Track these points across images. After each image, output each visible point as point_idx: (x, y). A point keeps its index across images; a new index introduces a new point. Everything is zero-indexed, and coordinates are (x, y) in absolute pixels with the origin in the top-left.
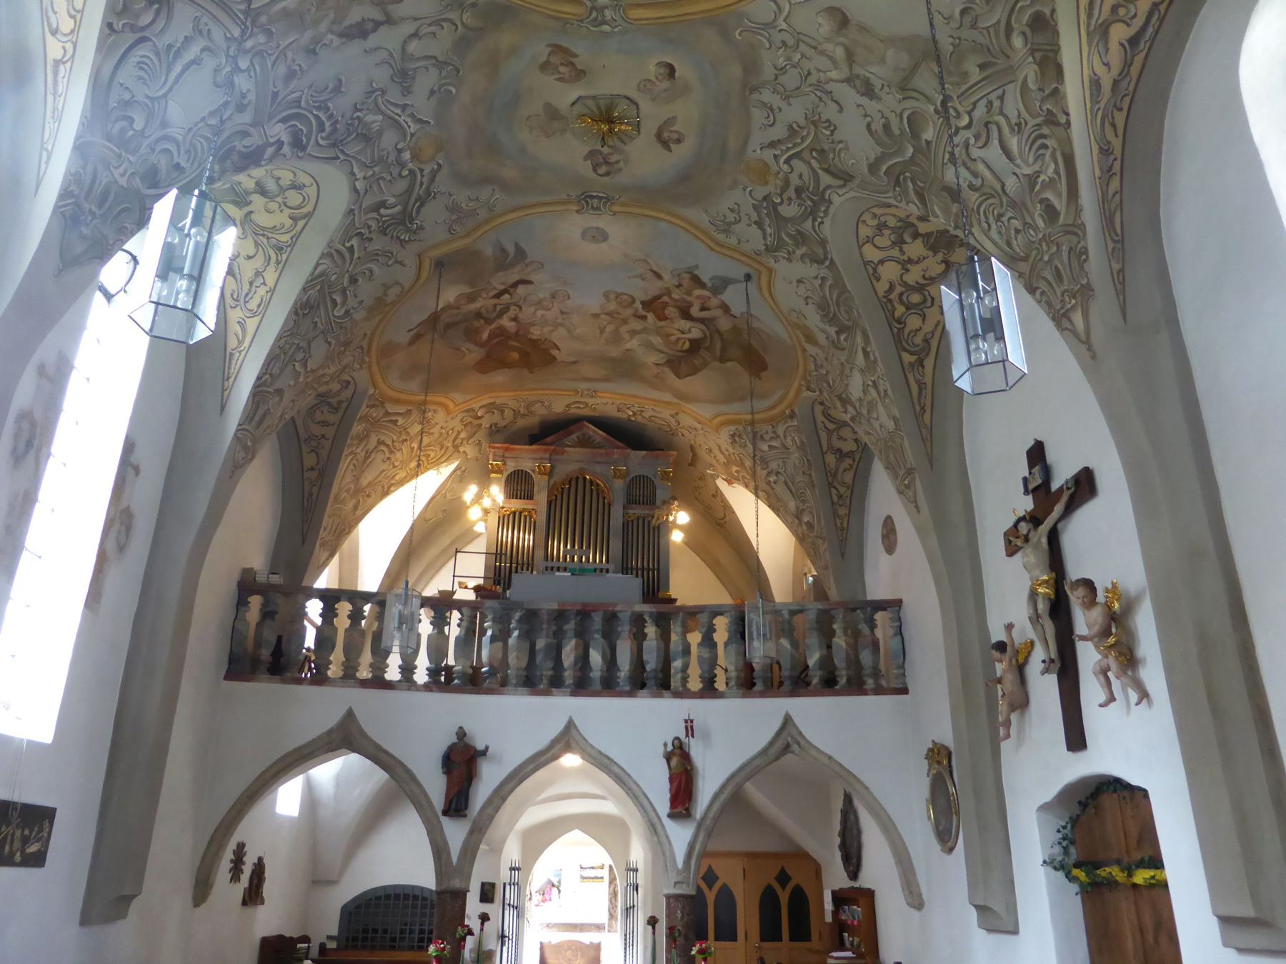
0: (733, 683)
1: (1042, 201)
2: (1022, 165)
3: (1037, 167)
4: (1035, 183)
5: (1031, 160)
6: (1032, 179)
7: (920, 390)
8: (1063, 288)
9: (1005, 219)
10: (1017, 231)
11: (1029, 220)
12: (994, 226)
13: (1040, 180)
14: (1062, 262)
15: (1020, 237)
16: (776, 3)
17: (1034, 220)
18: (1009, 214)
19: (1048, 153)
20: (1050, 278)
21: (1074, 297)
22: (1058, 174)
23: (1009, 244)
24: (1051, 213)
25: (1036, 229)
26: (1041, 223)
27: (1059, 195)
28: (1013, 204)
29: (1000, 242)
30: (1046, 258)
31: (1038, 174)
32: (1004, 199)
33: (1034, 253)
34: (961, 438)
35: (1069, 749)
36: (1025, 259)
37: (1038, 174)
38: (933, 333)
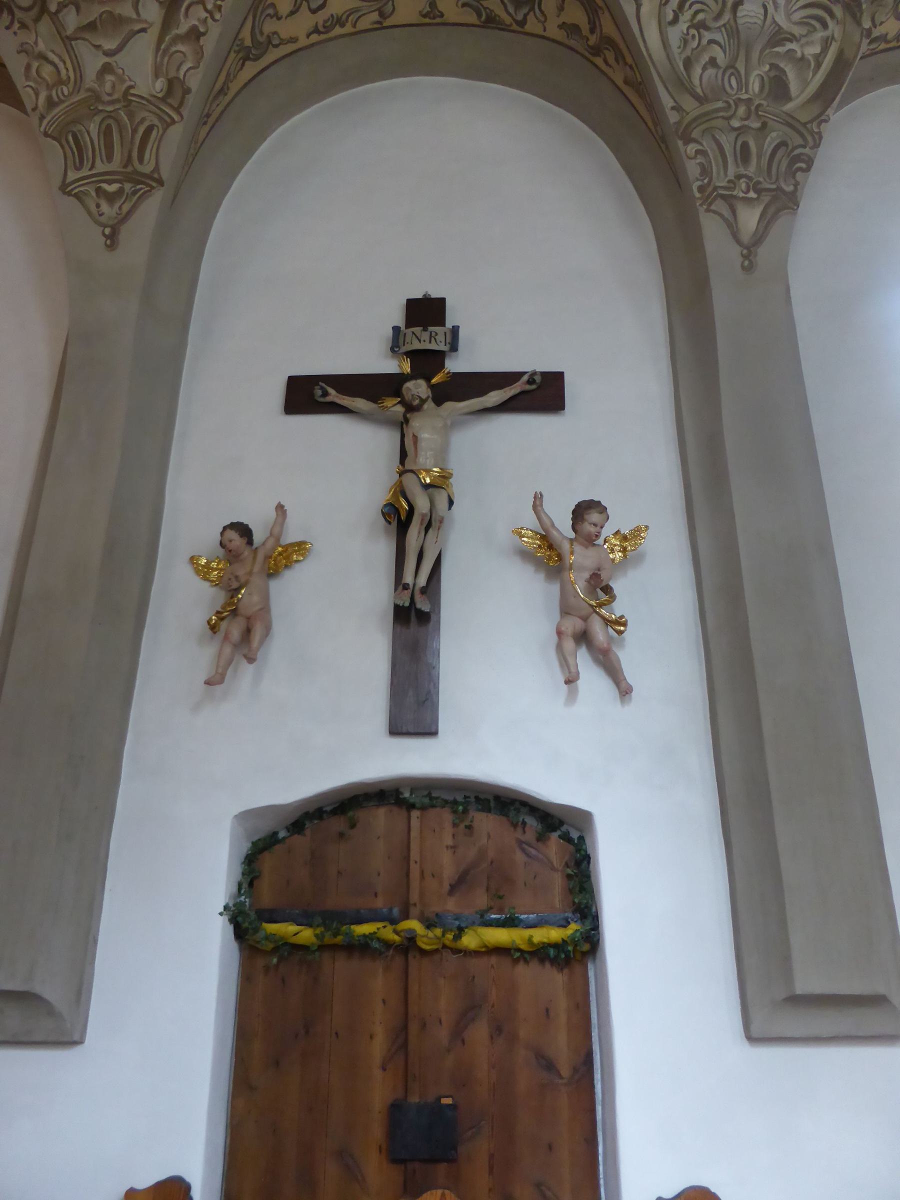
0: (114, 64)
1: (773, 66)
2: (782, 9)
3: (797, 31)
4: (780, 43)
5: (797, 17)
6: (779, 37)
7: (222, 90)
8: (742, 171)
9: (707, 36)
10: (713, 62)
11: (741, 66)
12: (683, 26)
13: (790, 46)
14: (760, 148)
15: (711, 71)
16: (544, 1196)
17: (747, 75)
18: (718, 37)
19: (820, 34)
20: (728, 149)
21: (758, 191)
22: (818, 65)
23: (688, 63)
24: (778, 88)
25: (743, 85)
26: (755, 86)
27: (805, 84)
28: (733, 32)
29: (675, 50)
30: (736, 123)
31: (792, 38)
32: (727, 16)
33: (720, 104)
34: (104, 884)
35: (291, 379)
36: (701, 100)
37: (792, 38)
38: (283, 42)
